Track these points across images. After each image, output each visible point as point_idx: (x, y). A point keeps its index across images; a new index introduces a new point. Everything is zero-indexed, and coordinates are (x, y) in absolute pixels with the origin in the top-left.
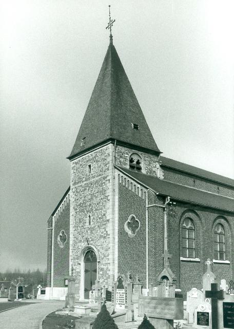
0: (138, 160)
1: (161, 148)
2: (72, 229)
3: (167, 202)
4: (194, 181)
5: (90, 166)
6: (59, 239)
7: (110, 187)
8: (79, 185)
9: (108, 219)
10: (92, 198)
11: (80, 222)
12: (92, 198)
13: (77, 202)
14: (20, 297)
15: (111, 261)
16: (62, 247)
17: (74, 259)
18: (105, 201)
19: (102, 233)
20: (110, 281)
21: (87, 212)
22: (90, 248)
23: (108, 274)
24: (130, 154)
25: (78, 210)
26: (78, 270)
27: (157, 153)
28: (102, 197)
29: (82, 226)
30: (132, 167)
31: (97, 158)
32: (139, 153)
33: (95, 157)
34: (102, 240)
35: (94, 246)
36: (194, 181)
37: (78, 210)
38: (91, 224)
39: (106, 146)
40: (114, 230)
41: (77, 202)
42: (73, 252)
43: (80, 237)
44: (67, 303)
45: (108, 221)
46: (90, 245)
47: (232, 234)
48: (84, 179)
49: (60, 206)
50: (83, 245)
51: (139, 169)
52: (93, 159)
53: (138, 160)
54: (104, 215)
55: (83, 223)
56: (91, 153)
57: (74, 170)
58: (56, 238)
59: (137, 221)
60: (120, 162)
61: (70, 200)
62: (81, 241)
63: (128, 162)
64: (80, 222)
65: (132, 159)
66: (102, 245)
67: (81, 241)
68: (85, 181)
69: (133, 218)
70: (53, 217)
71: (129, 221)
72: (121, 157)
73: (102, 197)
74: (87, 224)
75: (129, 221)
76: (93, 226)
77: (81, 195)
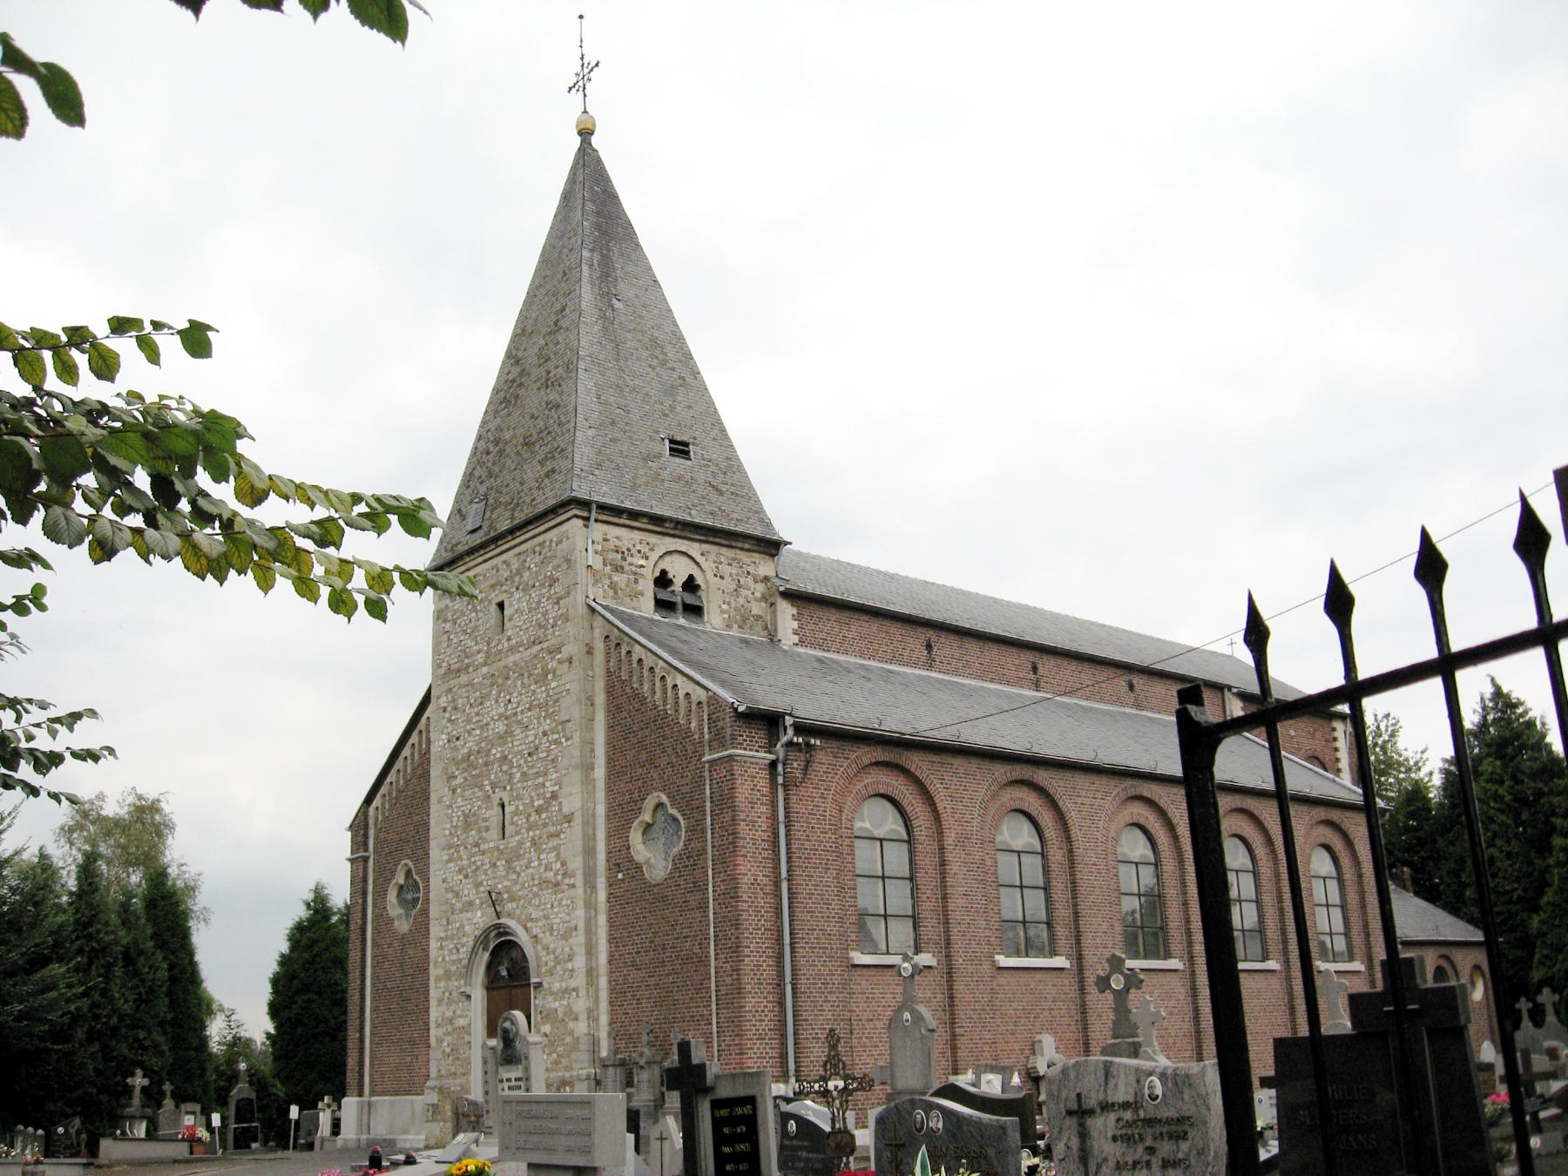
0: (691, 578)
1: (782, 531)
2: (436, 854)
3: (784, 739)
4: (929, 647)
5: (501, 606)
6: (392, 895)
7: (574, 687)
8: (464, 678)
9: (566, 810)
10: (509, 733)
11: (467, 826)
12: (509, 733)
13: (456, 749)
14: (464, 1121)
15: (580, 981)
16: (403, 926)
17: (448, 975)
18: (556, 742)
19: (548, 868)
20: (582, 1056)
21: (494, 786)
22: (501, 930)
23: (571, 1033)
24: (654, 556)
25: (459, 780)
26: (462, 1022)
27: (771, 546)
28: (547, 725)
29: (477, 845)
30: (663, 605)
31: (526, 574)
32: (694, 549)
33: (519, 572)
34: (547, 895)
35: (519, 921)
36: (929, 647)
37: (459, 780)
38: (509, 829)
39: (555, 531)
40: (589, 852)
41: (456, 749)
42: (441, 948)
43: (468, 891)
44: (808, 1094)
45: (569, 819)
46: (502, 921)
47: (171, 967)
48: (480, 658)
49: (388, 780)
50: (480, 918)
51: (695, 611)
52: (510, 578)
53: (691, 578)
54: (554, 796)
55: (479, 831)
56: (504, 557)
57: (445, 621)
58: (381, 893)
59: (675, 819)
60: (613, 586)
61: (429, 741)
62: (471, 903)
63: (647, 586)
64: (467, 826)
65: (664, 573)
66: (546, 917)
67: (471, 903)
68: (485, 664)
69: (659, 805)
70: (372, 810)
71: (647, 817)
72: (618, 569)
73: (547, 725)
74: (494, 834)
75: (647, 817)
76: (513, 842)
77: (469, 721)
